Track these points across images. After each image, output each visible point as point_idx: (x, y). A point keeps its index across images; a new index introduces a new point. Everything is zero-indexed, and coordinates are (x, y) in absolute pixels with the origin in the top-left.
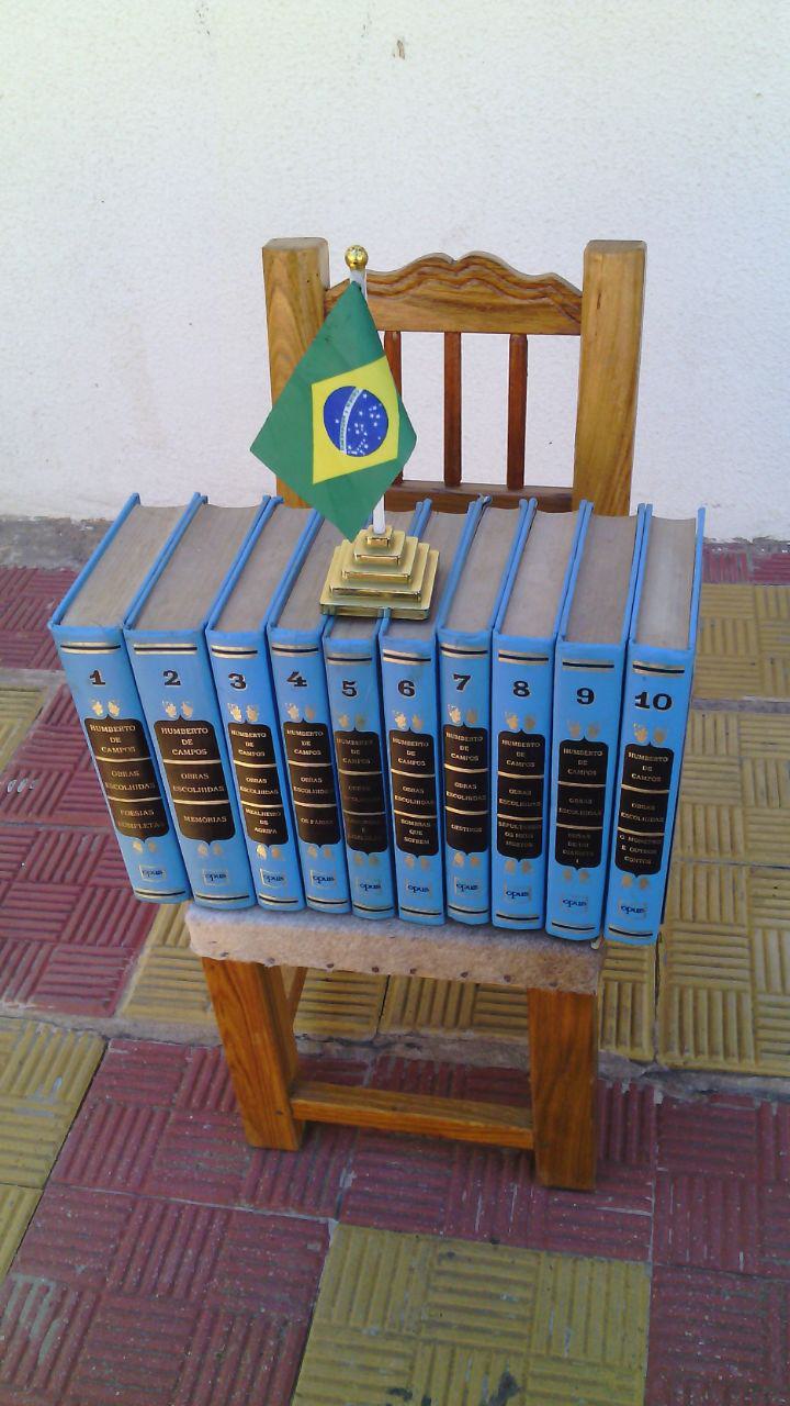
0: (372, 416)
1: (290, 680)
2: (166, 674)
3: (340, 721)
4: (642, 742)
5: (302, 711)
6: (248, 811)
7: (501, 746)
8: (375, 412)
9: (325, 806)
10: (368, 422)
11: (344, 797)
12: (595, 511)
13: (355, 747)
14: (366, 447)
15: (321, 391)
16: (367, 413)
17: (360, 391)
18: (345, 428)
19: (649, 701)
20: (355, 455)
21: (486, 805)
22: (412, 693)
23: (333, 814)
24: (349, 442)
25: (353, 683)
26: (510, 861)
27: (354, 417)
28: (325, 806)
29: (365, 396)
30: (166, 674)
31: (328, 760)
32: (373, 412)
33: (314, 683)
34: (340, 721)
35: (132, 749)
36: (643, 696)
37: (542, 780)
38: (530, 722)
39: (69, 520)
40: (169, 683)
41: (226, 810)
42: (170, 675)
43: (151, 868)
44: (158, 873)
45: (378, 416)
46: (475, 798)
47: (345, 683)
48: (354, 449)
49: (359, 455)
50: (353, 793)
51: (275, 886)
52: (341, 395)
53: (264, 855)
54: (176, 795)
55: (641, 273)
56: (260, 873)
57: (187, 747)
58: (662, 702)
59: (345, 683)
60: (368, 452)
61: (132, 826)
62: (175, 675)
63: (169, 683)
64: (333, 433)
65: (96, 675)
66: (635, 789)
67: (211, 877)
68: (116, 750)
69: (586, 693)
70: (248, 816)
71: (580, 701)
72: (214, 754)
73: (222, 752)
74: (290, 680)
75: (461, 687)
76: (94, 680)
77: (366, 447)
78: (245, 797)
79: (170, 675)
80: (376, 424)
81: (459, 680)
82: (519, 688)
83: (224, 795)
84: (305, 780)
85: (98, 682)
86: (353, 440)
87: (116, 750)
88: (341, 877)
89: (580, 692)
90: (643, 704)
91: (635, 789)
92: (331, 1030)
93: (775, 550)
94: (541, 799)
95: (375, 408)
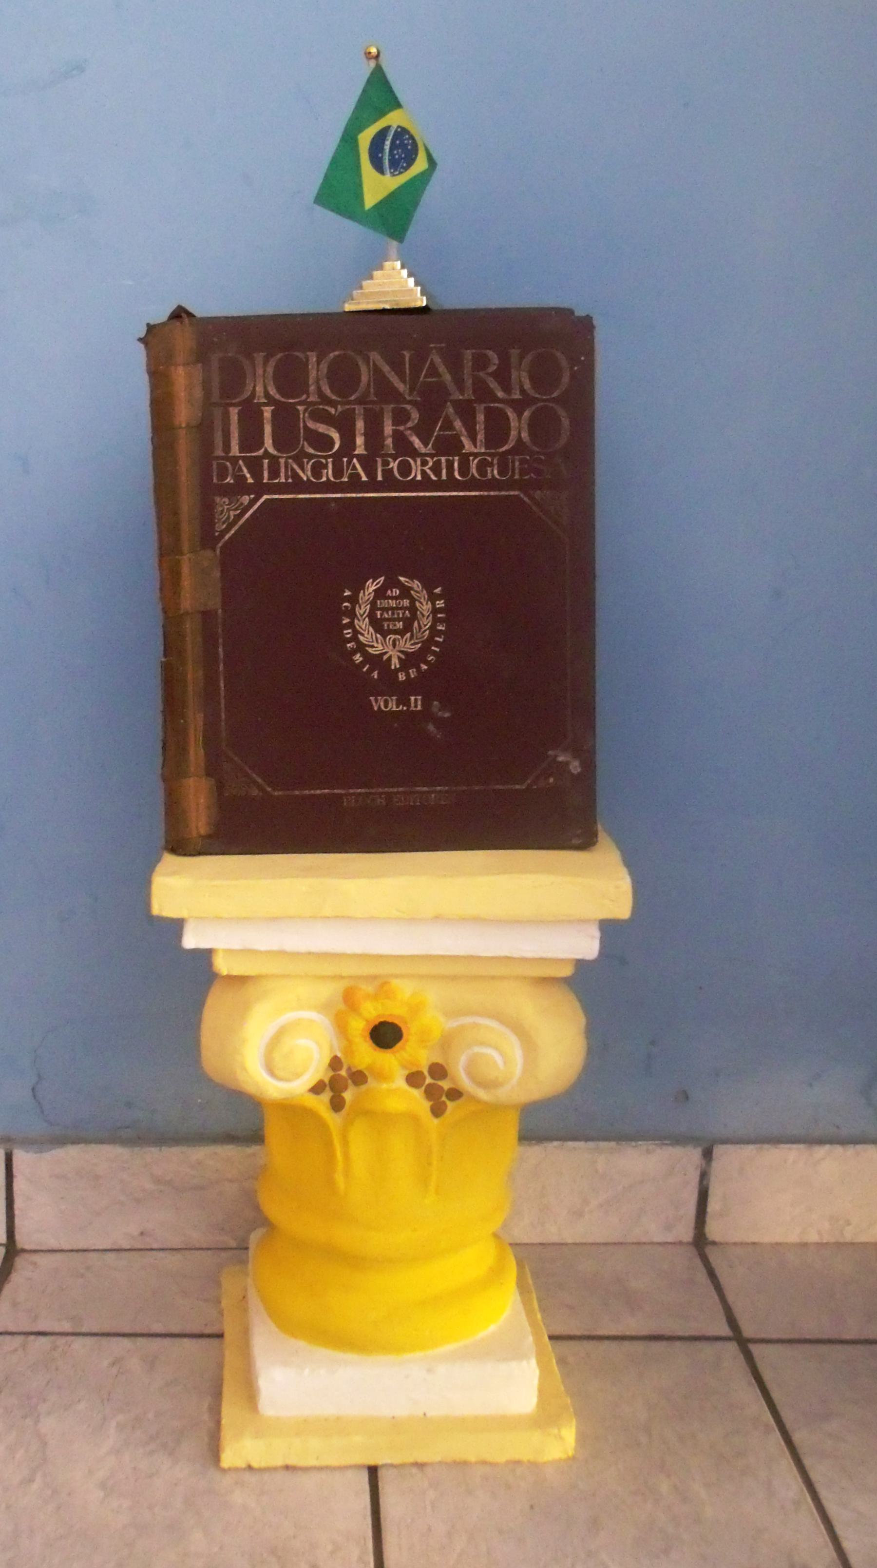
8: (408, 139)
10: (403, 146)
12: (450, 394)
14: (405, 165)
15: (365, 138)
16: (402, 142)
20: (397, 175)
27: (393, 146)
39: (571, 312)
48: (396, 170)
49: (400, 173)
52: (382, 135)
55: (353, 851)
60: (406, 169)
64: (378, 166)
77: (405, 165)
80: (409, 147)
81: (326, 1096)
92: (350, 977)
93: (166, 706)
95: (407, 136)
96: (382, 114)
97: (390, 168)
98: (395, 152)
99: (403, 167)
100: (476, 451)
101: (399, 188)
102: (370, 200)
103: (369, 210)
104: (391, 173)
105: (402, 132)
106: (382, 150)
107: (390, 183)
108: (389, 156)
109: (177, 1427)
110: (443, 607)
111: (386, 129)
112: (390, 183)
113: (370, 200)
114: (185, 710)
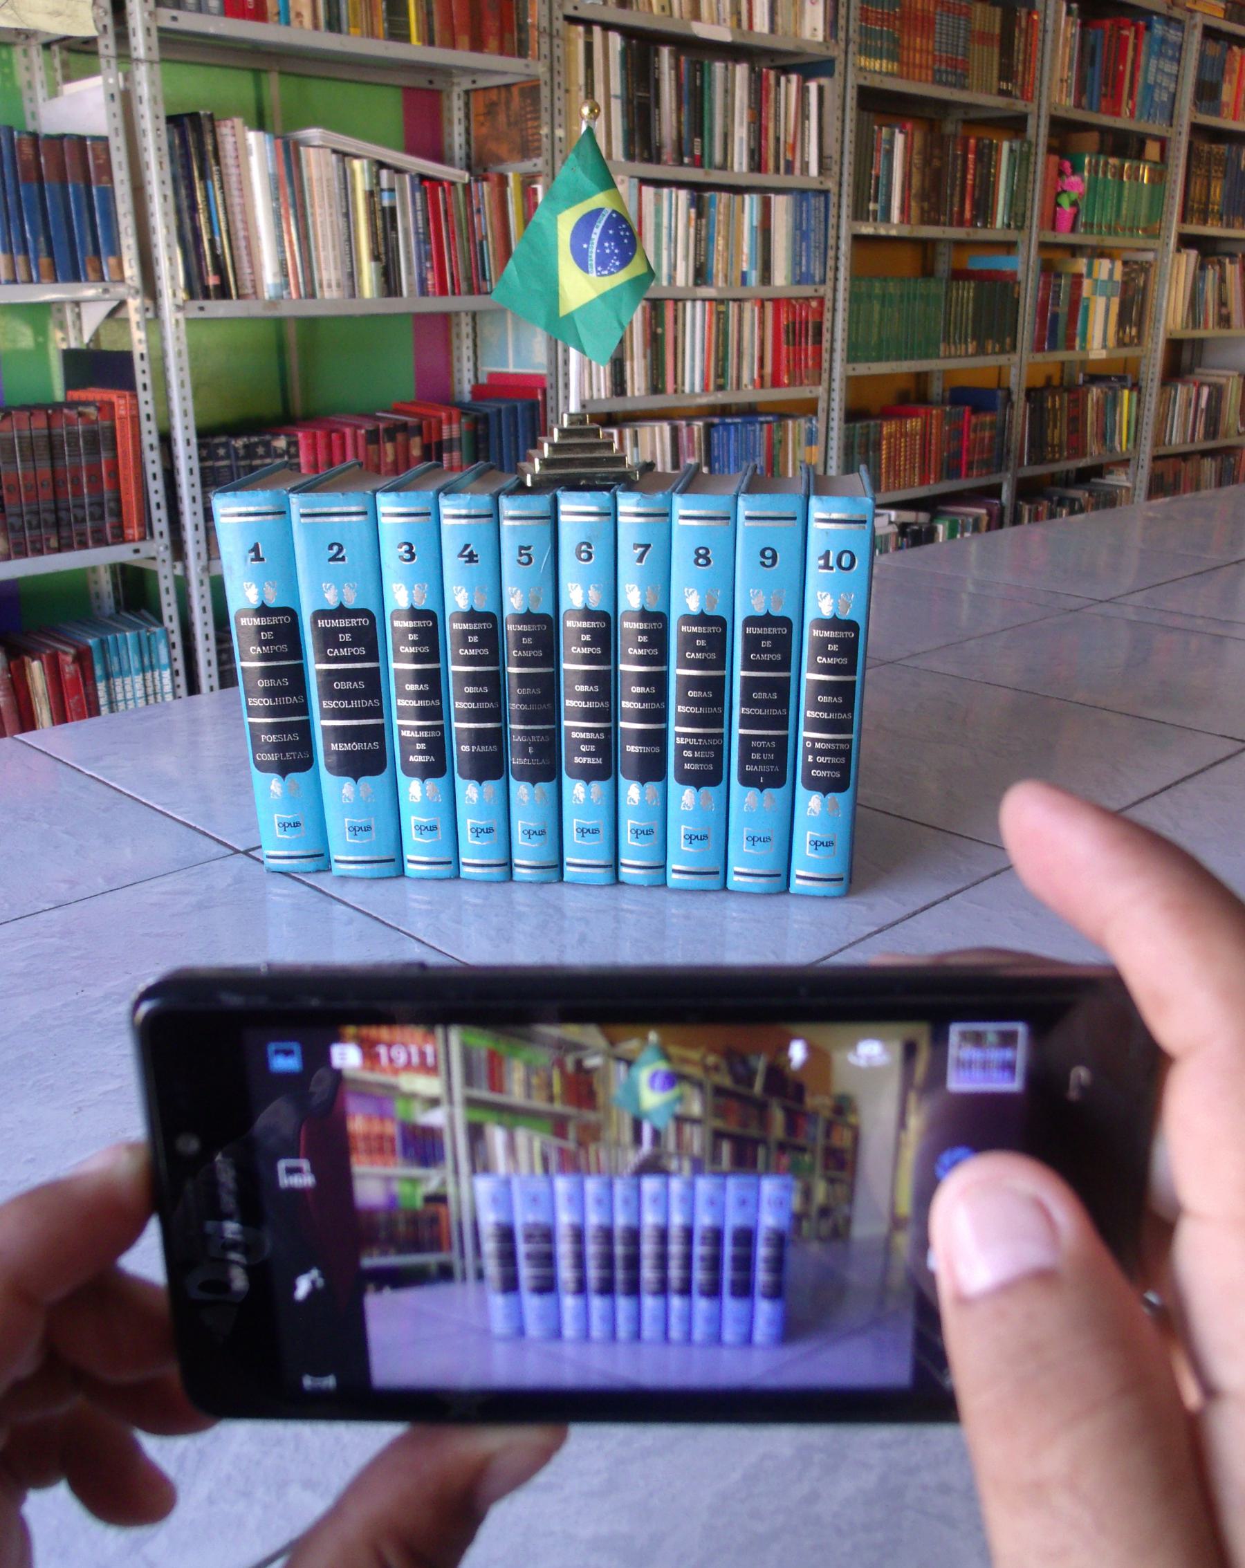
0: (622, 233)
1: (461, 555)
2: (331, 547)
3: (512, 600)
4: (760, 611)
5: (471, 597)
6: (404, 733)
7: (746, 637)
8: (625, 230)
9: (489, 725)
11: (513, 706)
13: (472, 633)
17: (610, 211)
18: (594, 250)
19: (832, 562)
21: (304, 708)
22: (590, 557)
23: (497, 737)
24: (598, 264)
25: (529, 548)
26: (752, 792)
28: (489, 725)
29: (614, 215)
30: (331, 547)
31: (497, 664)
32: (623, 229)
33: (485, 557)
34: (512, 600)
35: (284, 648)
36: (826, 556)
37: (723, 677)
38: (711, 601)
40: (333, 559)
41: (378, 734)
42: (336, 548)
43: (288, 818)
44: (297, 825)
45: (622, 233)
46: (773, 712)
47: (521, 548)
50: (523, 699)
51: (363, 840)
53: (582, 796)
54: (326, 714)
56: (411, 820)
57: (345, 645)
58: (845, 561)
59: (521, 548)
61: (272, 757)
62: (341, 549)
63: (333, 559)
65: (256, 549)
66: (275, 664)
67: (355, 830)
68: (344, 652)
69: (768, 553)
70: (402, 739)
71: (763, 564)
72: (373, 655)
73: (442, 658)
74: (461, 555)
75: (640, 559)
76: (253, 554)
78: (403, 713)
79: (336, 548)
80: (626, 241)
81: (640, 550)
82: (700, 556)
83: (377, 712)
84: (692, 694)
85: (258, 558)
86: (603, 262)
87: (344, 652)
88: (605, 832)
89: (762, 554)
90: (827, 566)
91: (275, 664)
94: (722, 706)
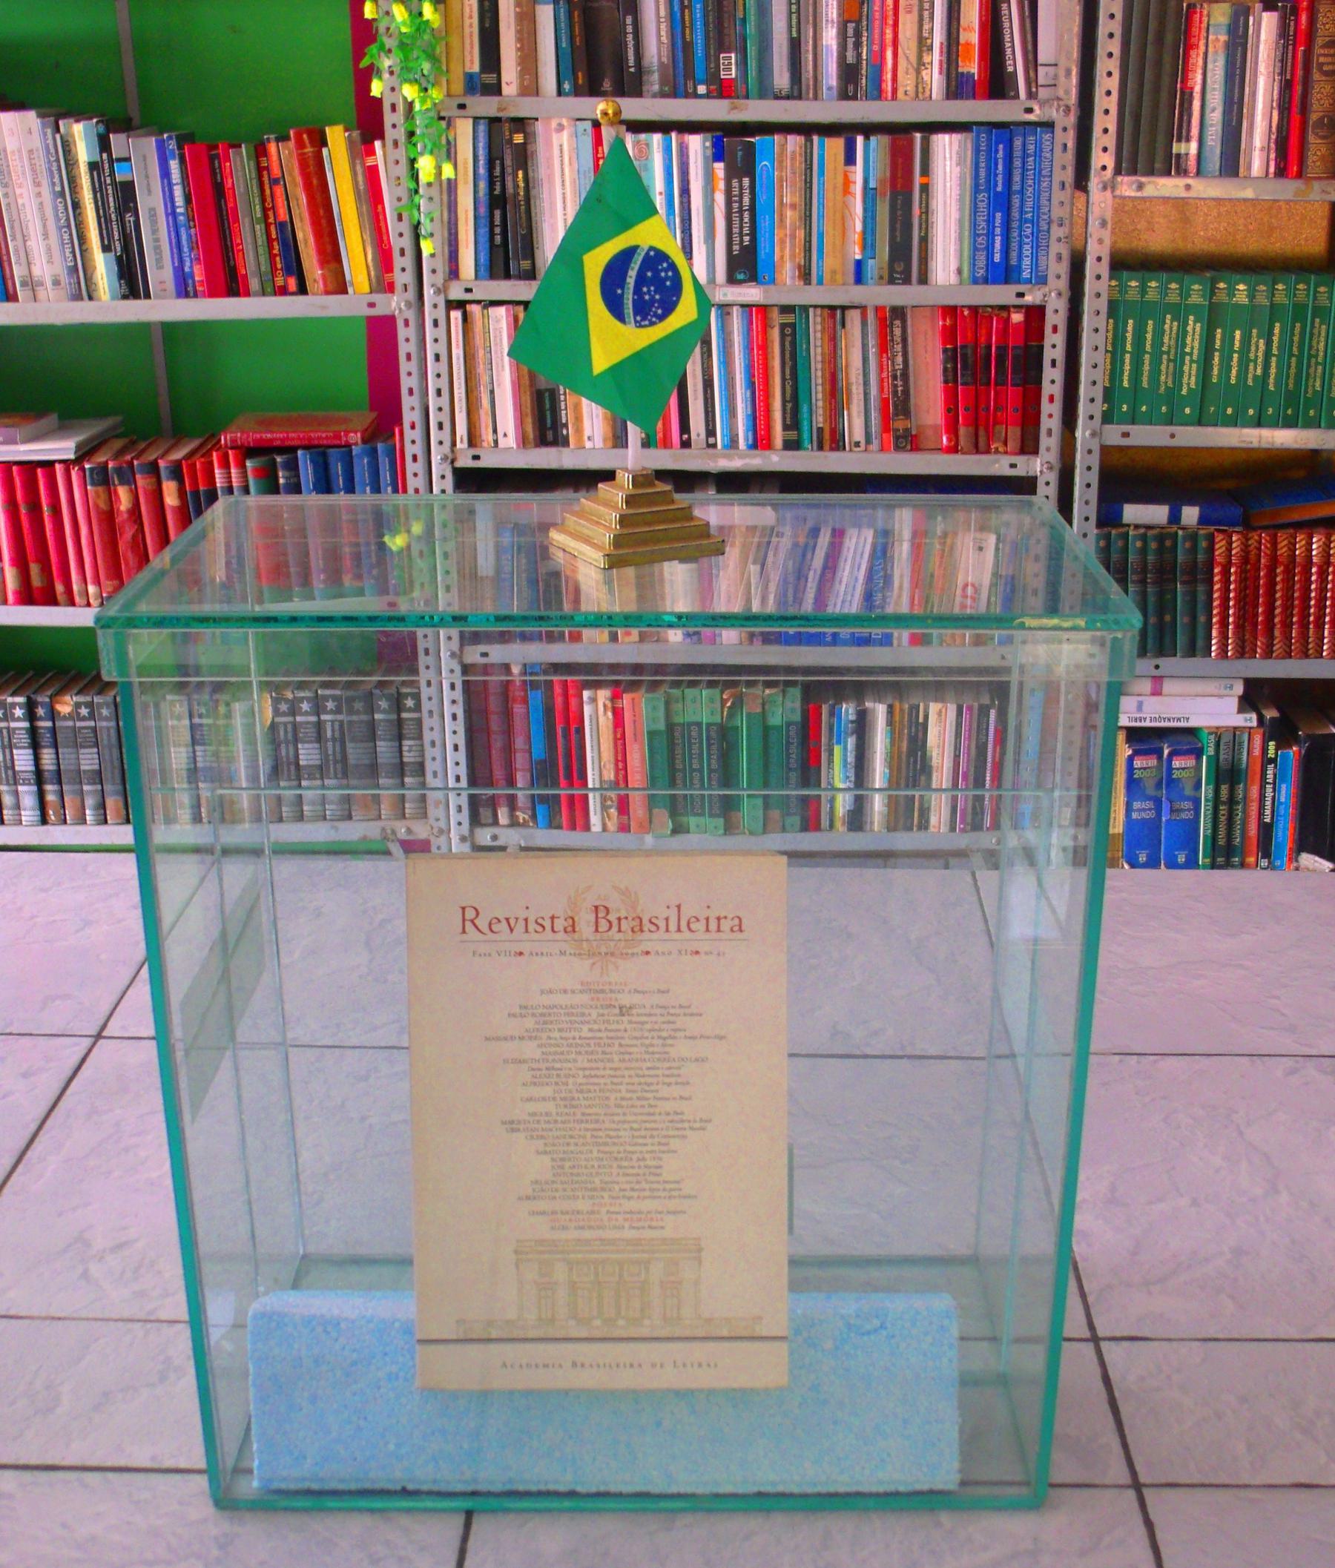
8: (666, 270)
10: (658, 282)
14: (660, 311)
15: (596, 261)
16: (656, 272)
27: (641, 280)
48: (644, 319)
49: (652, 324)
60: (662, 318)
64: (615, 306)
77: (660, 311)
96: (626, 225)
97: (635, 315)
98: (645, 289)
99: (655, 315)
100: (1320, 41)
101: (651, 346)
102: (600, 363)
103: (599, 375)
104: (636, 321)
105: (657, 259)
106: (622, 284)
107: (629, 339)
108: (635, 293)
109: (1092, 656)
110: (874, 781)
111: (628, 254)
112: (629, 339)
113: (600, 363)
114: (948, 322)
